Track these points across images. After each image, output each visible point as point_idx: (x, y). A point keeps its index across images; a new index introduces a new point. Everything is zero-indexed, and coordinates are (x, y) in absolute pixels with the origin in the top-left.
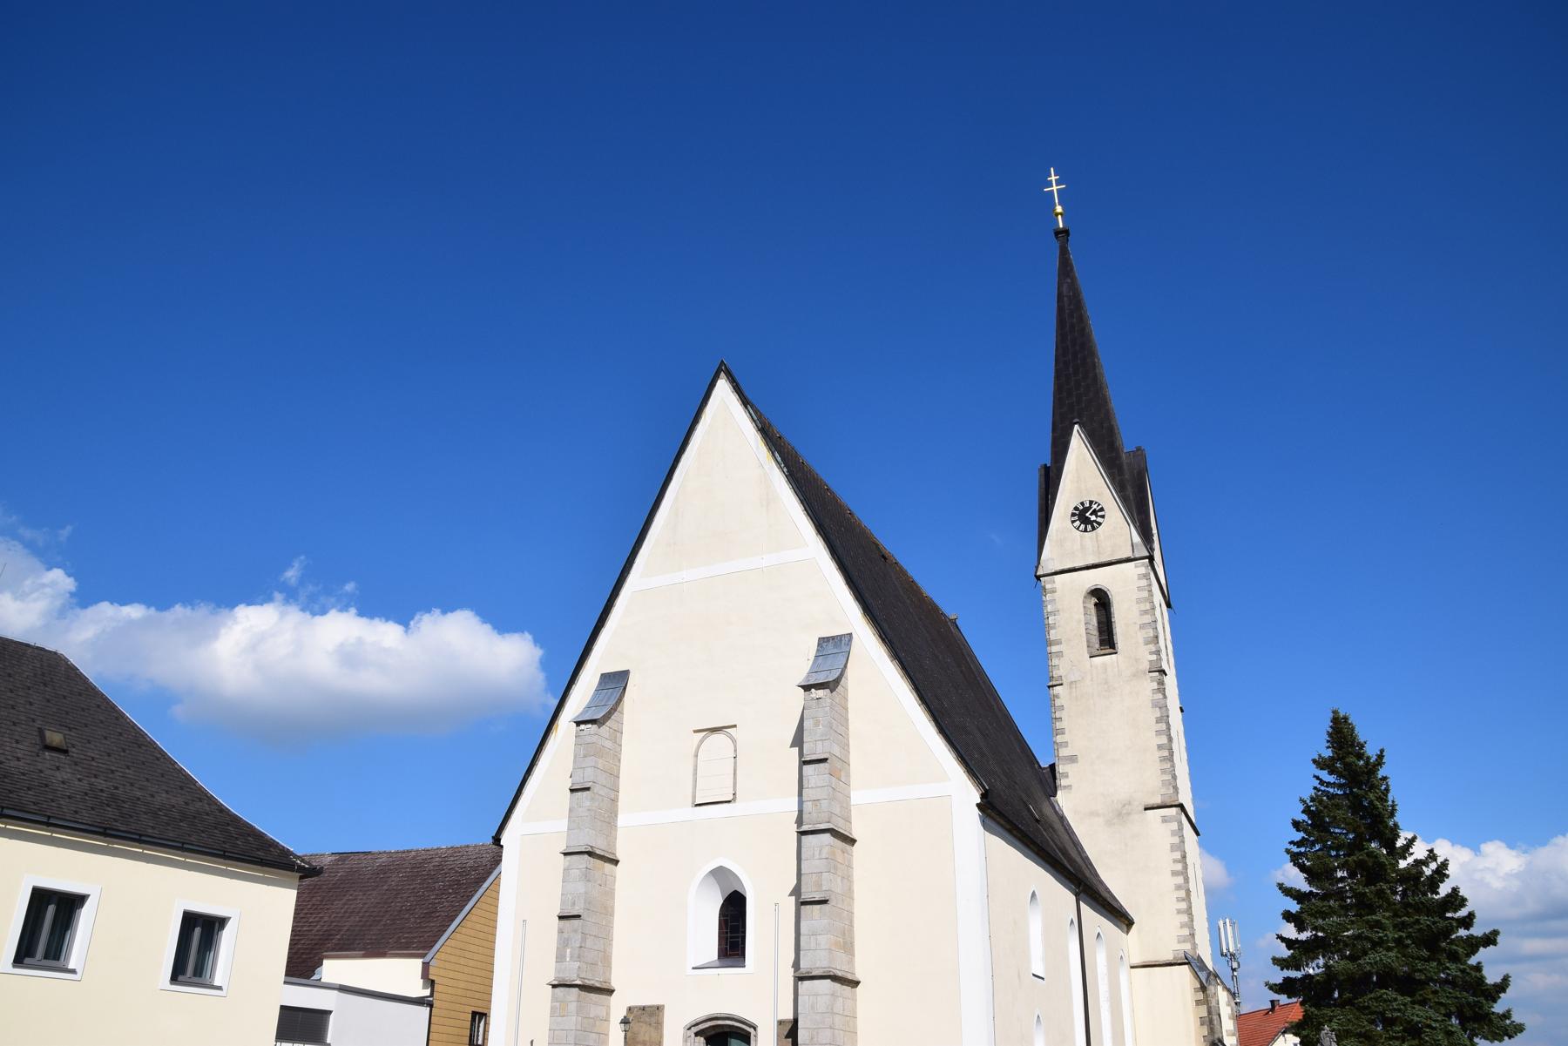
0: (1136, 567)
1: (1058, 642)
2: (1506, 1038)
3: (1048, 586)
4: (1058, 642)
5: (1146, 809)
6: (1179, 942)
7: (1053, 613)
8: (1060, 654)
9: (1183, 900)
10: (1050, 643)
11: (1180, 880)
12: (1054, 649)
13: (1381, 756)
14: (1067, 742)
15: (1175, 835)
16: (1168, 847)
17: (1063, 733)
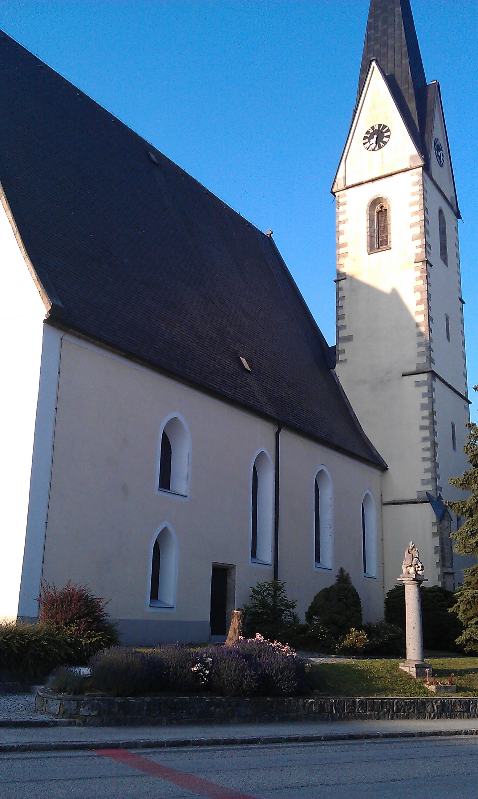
0: (412, 175)
1: (345, 245)
2: (388, 467)
3: (341, 200)
4: (345, 245)
5: (403, 376)
6: (423, 484)
7: (344, 222)
8: (345, 255)
9: (428, 449)
10: (339, 246)
11: (427, 433)
12: (342, 251)
13: (345, 361)
14: (345, 326)
15: (426, 396)
16: (419, 407)
17: (343, 318)
